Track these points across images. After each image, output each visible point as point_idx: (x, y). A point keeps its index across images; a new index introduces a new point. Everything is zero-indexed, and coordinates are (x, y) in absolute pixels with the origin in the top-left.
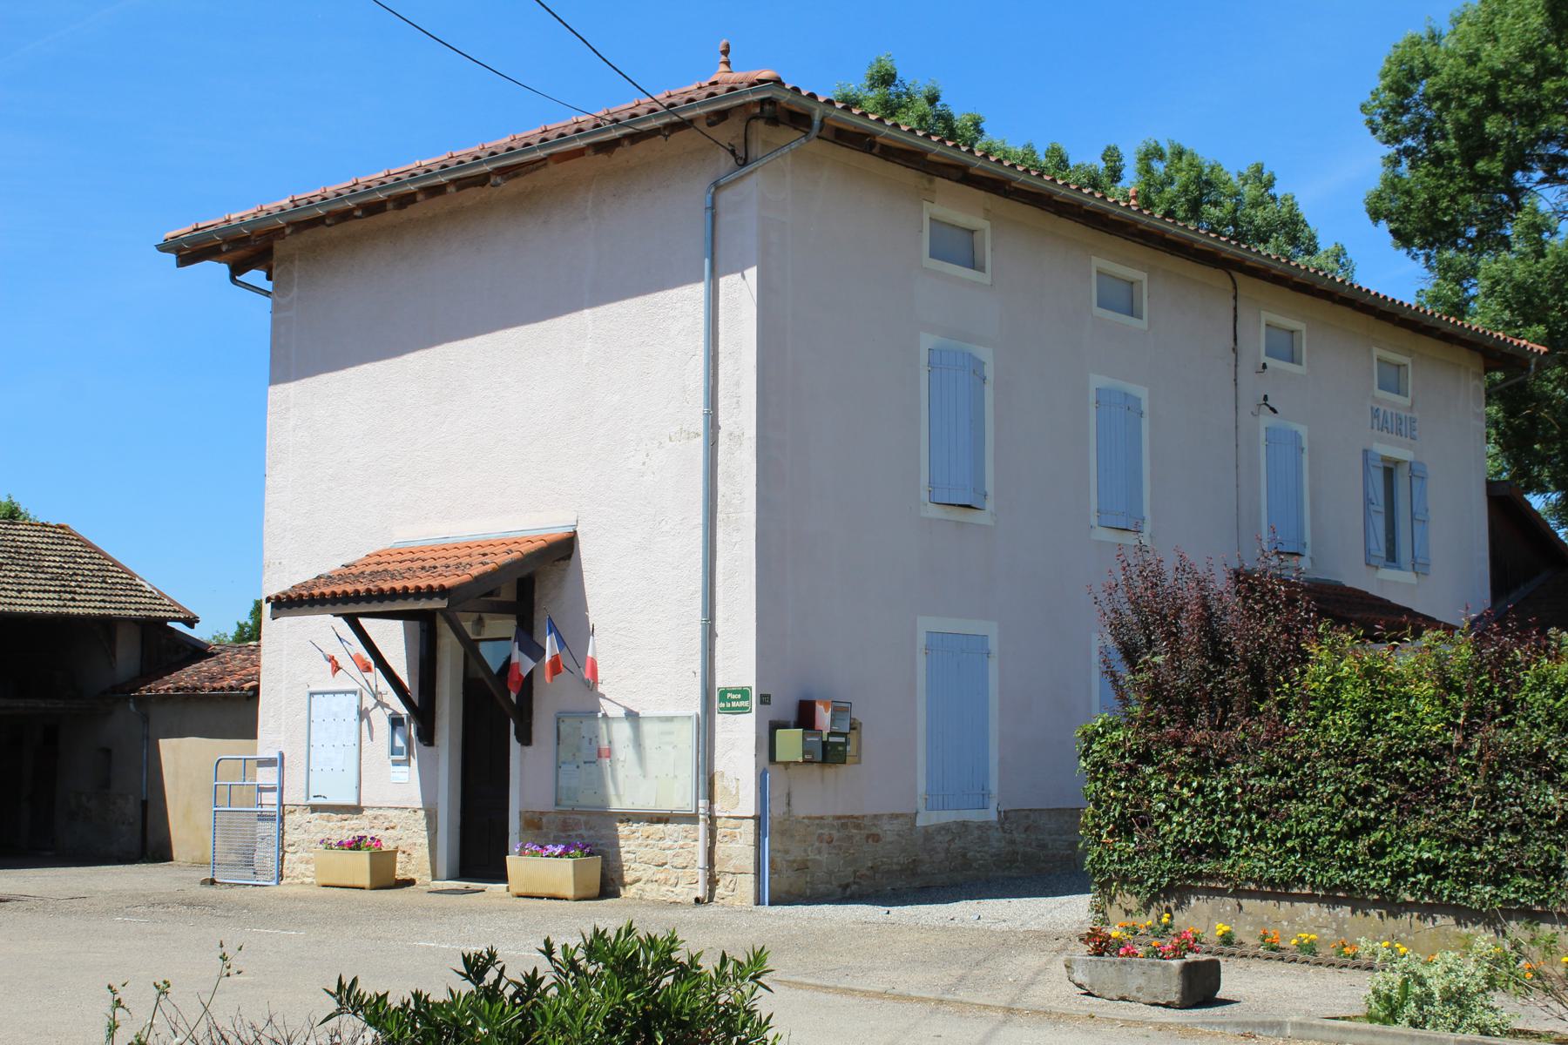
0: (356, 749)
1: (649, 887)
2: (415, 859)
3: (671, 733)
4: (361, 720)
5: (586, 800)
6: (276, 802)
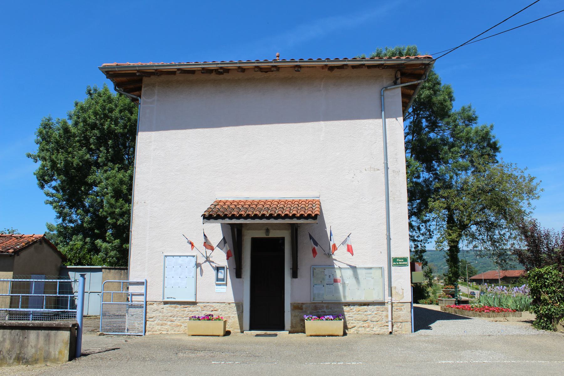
0: (194, 279)
1: (360, 329)
2: (233, 323)
3: (371, 273)
4: (197, 268)
5: (328, 298)
6: (144, 300)
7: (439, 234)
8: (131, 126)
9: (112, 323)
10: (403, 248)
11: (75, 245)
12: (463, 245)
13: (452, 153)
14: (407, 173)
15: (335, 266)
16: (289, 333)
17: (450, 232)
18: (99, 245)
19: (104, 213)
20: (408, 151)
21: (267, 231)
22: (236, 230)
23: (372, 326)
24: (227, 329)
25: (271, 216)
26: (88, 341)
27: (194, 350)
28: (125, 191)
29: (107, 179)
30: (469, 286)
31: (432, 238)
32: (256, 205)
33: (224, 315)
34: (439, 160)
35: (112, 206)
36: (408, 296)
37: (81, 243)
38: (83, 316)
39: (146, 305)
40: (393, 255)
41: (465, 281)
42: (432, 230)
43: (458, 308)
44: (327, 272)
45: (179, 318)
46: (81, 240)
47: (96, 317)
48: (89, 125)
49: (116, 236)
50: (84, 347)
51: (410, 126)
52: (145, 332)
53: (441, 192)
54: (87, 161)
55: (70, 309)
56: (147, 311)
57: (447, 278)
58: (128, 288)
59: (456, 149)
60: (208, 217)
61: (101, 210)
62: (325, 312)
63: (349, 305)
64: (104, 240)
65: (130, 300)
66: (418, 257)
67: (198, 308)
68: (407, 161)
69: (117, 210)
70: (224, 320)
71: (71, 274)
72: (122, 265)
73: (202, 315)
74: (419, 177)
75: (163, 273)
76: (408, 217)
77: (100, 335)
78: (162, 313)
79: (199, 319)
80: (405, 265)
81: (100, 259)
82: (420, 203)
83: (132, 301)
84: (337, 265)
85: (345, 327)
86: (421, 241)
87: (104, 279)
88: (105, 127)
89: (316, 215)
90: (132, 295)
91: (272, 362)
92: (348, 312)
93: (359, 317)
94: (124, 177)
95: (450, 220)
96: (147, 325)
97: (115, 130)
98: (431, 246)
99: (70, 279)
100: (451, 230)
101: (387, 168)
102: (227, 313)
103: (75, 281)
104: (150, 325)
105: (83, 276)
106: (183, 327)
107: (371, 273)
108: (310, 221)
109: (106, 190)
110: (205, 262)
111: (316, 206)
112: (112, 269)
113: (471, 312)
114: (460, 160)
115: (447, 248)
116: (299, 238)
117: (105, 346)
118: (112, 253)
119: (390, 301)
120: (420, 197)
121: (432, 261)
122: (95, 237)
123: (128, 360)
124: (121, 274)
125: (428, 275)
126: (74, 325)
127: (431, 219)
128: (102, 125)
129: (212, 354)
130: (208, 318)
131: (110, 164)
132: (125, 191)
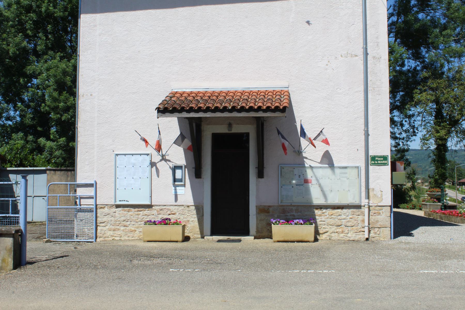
0: (148, 180)
3: (346, 173)
4: (152, 167)
5: (297, 200)
6: (94, 203)
7: (424, 131)
8: (72, 9)
9: (59, 227)
10: (383, 146)
11: (15, 144)
12: (453, 143)
13: (444, 37)
14: (390, 60)
15: (306, 165)
16: (255, 238)
17: (438, 128)
18: (42, 144)
19: (47, 108)
20: (392, 35)
21: (230, 125)
22: (194, 125)
23: (346, 232)
24: (186, 234)
25: (234, 109)
26: (32, 247)
27: (150, 256)
28: (69, 83)
29: (48, 70)
30: (458, 190)
31: (416, 135)
32: (217, 97)
33: (182, 219)
34: (428, 46)
35: (55, 100)
36: (388, 199)
37: (22, 142)
38: (27, 223)
39: (96, 209)
40: (371, 153)
41: (453, 184)
42: (416, 126)
43: (444, 213)
44: (296, 171)
45: (133, 223)
46: (22, 139)
47: (42, 224)
48: (23, 7)
49: (61, 133)
50: (29, 256)
51: (394, 6)
52: (96, 238)
53: (429, 82)
54: (24, 49)
55: (12, 214)
56: (98, 215)
57: (432, 180)
58: (75, 191)
59: (448, 31)
60: (164, 110)
61: (43, 105)
62: (294, 215)
63: (321, 208)
64: (48, 139)
65: (78, 203)
66: (400, 157)
67: (154, 211)
68: (389, 47)
69: (62, 104)
70: (183, 224)
71: (12, 176)
72: (68, 166)
73: (158, 219)
74: (403, 65)
75: (114, 173)
76: (389, 111)
77: (47, 242)
78: (115, 217)
79: (155, 223)
80: (385, 164)
81: (43, 160)
82: (402, 95)
83: (80, 205)
84: (308, 163)
85: (317, 232)
86: (403, 139)
87: (48, 181)
88: (43, 10)
89: (285, 108)
90: (81, 198)
91: (235, 270)
92: (320, 215)
93: (332, 221)
94: (67, 67)
95: (439, 115)
96: (98, 231)
97: (55, 13)
98: (415, 144)
99: (11, 181)
100: (439, 126)
101: (366, 54)
102: (185, 216)
103: (17, 183)
104: (102, 230)
105: (24, 177)
106: (137, 232)
107: (346, 173)
108: (277, 114)
109: (47, 82)
110: (161, 161)
111: (285, 97)
112: (58, 170)
113: (459, 218)
114: (453, 45)
115: (433, 147)
116: (265, 133)
117: (52, 253)
118: (57, 153)
119: (367, 204)
120: (403, 89)
121: (416, 162)
122: (38, 135)
123: (77, 269)
124: (68, 176)
125: (411, 177)
126: (17, 231)
127: (417, 113)
128: (39, 7)
129: (169, 261)
130: (165, 222)
131: (51, 52)
132: (69, 83)
